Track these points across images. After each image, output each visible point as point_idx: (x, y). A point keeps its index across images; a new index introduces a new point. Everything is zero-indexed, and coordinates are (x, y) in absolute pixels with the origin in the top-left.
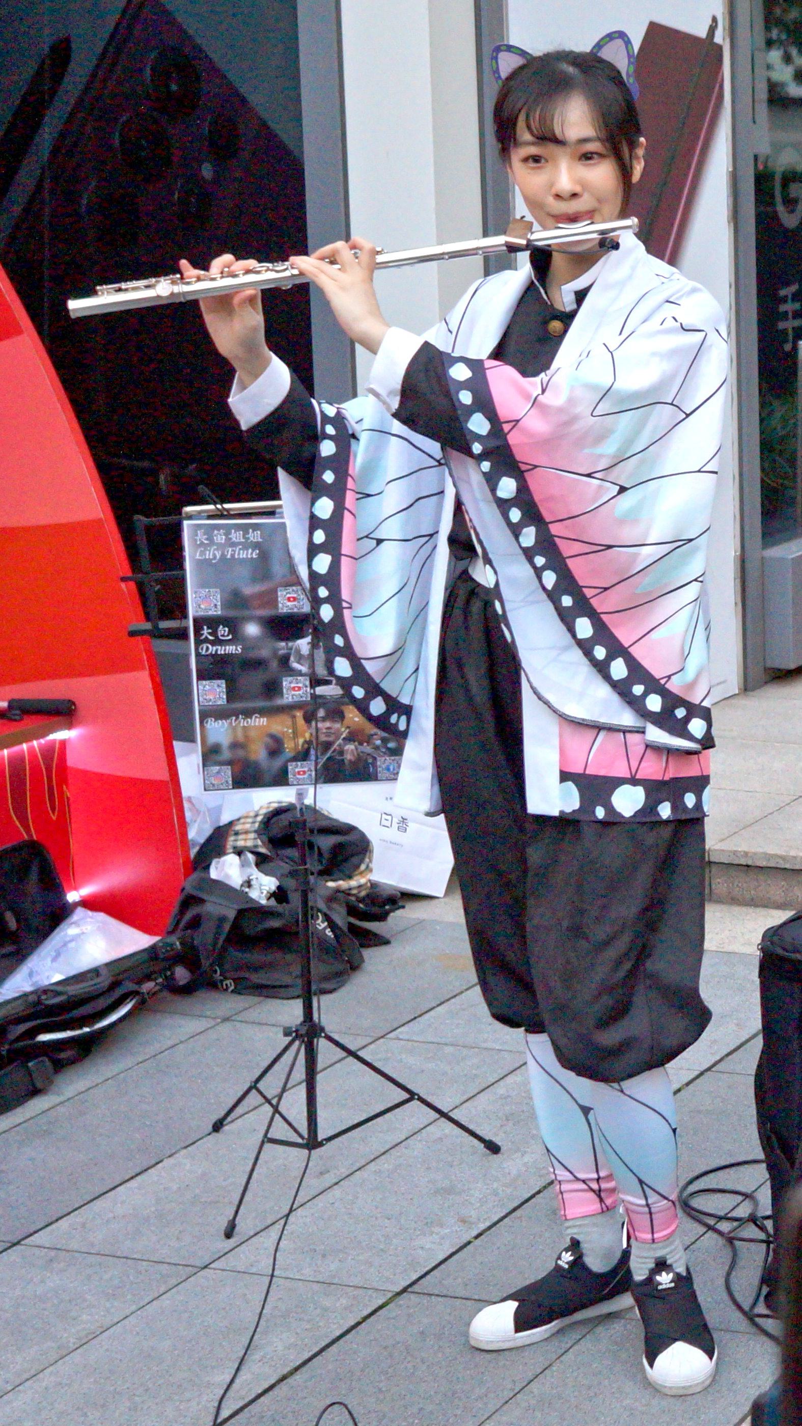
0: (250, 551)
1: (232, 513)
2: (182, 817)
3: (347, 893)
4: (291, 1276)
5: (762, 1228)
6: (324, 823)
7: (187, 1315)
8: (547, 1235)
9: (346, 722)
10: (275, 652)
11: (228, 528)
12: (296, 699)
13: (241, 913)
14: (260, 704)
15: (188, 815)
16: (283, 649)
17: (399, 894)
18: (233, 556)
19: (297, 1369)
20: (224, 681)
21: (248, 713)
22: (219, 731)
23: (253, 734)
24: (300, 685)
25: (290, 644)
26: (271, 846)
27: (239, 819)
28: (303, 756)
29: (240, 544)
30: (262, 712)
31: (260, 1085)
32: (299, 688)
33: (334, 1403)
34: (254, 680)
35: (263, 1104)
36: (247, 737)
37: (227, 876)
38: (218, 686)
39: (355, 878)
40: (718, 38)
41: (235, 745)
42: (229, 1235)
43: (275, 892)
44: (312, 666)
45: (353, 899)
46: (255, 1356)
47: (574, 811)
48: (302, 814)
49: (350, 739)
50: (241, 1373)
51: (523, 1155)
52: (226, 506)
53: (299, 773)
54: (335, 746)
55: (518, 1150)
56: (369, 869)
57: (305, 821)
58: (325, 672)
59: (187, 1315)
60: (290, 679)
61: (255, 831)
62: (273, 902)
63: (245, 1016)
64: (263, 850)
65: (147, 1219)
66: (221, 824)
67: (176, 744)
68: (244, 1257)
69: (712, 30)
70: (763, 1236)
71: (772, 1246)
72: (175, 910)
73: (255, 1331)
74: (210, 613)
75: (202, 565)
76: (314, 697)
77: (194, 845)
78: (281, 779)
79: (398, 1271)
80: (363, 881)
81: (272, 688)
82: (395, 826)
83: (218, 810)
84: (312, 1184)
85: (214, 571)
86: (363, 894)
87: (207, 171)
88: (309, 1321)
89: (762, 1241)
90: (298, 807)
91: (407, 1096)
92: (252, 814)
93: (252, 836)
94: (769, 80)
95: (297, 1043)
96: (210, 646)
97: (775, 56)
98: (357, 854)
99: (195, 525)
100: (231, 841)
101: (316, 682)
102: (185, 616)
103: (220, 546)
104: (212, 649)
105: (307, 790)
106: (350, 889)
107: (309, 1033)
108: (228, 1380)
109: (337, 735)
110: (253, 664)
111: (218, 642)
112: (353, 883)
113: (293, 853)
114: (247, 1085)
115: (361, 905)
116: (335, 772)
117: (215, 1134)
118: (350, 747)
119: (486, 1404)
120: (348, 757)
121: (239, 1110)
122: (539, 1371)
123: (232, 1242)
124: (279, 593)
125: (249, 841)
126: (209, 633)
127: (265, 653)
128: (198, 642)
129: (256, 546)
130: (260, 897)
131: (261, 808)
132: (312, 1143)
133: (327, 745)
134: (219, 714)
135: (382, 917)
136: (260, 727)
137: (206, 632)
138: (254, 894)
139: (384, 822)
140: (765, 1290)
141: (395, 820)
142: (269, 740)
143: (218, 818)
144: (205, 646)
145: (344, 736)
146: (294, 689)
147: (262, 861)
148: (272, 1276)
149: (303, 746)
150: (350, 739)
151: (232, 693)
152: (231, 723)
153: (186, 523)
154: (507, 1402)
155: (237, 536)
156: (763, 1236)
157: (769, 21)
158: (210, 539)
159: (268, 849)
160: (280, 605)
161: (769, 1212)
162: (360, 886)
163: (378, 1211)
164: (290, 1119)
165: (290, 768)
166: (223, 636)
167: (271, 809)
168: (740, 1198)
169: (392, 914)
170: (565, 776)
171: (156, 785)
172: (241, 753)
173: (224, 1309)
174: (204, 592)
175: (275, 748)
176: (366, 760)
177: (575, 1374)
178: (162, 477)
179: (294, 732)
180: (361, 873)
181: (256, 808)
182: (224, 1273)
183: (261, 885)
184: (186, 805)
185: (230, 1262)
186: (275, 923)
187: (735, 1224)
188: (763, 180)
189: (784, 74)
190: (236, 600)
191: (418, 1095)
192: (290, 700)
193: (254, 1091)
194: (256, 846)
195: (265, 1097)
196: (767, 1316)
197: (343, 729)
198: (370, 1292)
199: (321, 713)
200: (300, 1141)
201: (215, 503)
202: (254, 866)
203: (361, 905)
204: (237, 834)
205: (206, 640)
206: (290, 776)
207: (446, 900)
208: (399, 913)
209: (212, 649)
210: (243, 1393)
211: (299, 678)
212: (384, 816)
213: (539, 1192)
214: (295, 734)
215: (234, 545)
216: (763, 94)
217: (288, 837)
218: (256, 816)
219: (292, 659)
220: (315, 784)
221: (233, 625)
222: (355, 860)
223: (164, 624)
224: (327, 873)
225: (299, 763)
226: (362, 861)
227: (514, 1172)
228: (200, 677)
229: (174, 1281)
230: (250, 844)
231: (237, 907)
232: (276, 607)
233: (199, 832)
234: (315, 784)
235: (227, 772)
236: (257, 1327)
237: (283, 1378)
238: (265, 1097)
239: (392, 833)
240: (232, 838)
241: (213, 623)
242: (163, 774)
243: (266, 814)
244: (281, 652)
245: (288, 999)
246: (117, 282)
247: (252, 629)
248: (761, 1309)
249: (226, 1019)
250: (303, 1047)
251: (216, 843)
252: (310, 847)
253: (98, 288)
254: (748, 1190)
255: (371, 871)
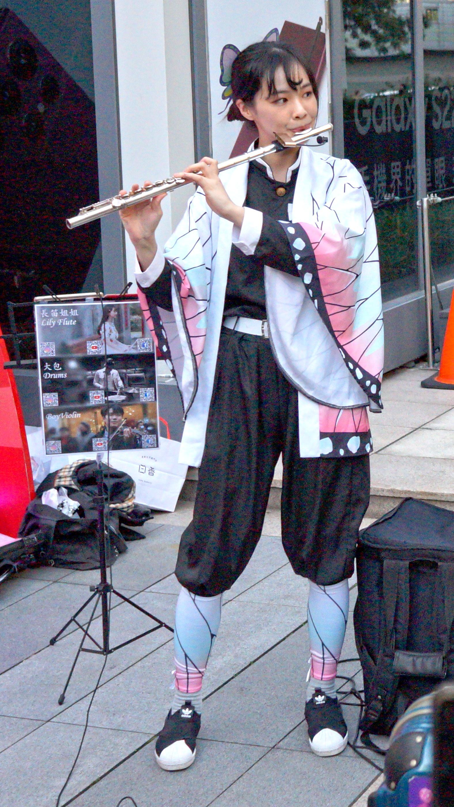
0: (71, 321)
1: (62, 300)
2: (30, 469)
3: (121, 510)
4: (97, 726)
5: (359, 698)
6: (111, 472)
7: (39, 748)
8: (238, 702)
9: (125, 415)
10: (85, 378)
11: (59, 309)
12: (97, 403)
13: (58, 522)
14: (79, 406)
15: (32, 466)
16: (90, 375)
17: (150, 511)
18: (62, 323)
19: (101, 778)
20: (57, 393)
21: (70, 411)
22: (55, 421)
23: (73, 423)
24: (99, 395)
25: (94, 372)
26: (79, 485)
27: (61, 470)
28: (100, 435)
29: (65, 317)
30: (79, 410)
31: (76, 619)
32: (99, 397)
33: (127, 797)
34: (73, 393)
35: (77, 629)
36: (70, 425)
37: (51, 501)
38: (54, 396)
39: (126, 502)
40: (323, 29)
41: (63, 429)
42: (61, 703)
43: (77, 510)
44: (106, 384)
45: (125, 513)
46: (77, 771)
47: (330, 453)
48: (100, 467)
49: (127, 425)
50: (70, 781)
51: (223, 658)
52: (59, 296)
53: (98, 444)
54: (118, 429)
55: (220, 654)
56: (133, 497)
57: (102, 471)
58: (113, 388)
59: (39, 748)
60: (93, 392)
61: (71, 476)
62: (77, 516)
63: (66, 579)
64: (74, 487)
65: (15, 694)
66: (51, 472)
67: (27, 428)
68: (69, 715)
69: (320, 24)
70: (359, 702)
71: (364, 708)
72: (23, 521)
73: (77, 757)
74: (49, 355)
75: (44, 328)
76: (107, 402)
77: (37, 483)
78: (89, 448)
79: (155, 723)
80: (130, 504)
81: (84, 397)
82: (147, 472)
83: (49, 463)
84: (108, 674)
85: (51, 332)
86: (130, 511)
87: (41, 108)
88: (106, 751)
89: (358, 705)
90: (98, 463)
91: (158, 624)
92: (69, 467)
93: (69, 479)
94: (346, 48)
95: (97, 595)
96: (49, 374)
97: (348, 34)
98: (126, 488)
99: (42, 307)
100: (57, 483)
101: (108, 393)
102: (35, 357)
103: (54, 318)
104: (51, 376)
105: (103, 454)
106: (123, 508)
107: (104, 589)
108: (63, 785)
109: (120, 422)
110: (73, 383)
111: (53, 371)
112: (125, 505)
113: (94, 489)
114: (69, 619)
115: (129, 517)
116: (119, 443)
117: (51, 646)
118: (127, 430)
119: (207, 797)
120: (126, 435)
121: (65, 633)
122: (236, 779)
123: (63, 707)
124: (88, 344)
125: (67, 481)
126: (49, 367)
127: (79, 378)
128: (43, 372)
129: (75, 318)
130: (69, 513)
131: (73, 463)
132: (106, 651)
133: (114, 429)
134: (54, 411)
135: (141, 524)
136: (77, 418)
137: (47, 366)
138: (65, 511)
139: (141, 470)
140: (361, 733)
141: (147, 469)
142: (81, 426)
143: (49, 469)
144: (46, 374)
145: (123, 423)
146: (95, 397)
147: (71, 492)
148: (87, 726)
149: (100, 429)
150: (127, 425)
151: (61, 401)
152: (61, 416)
153: (36, 306)
154: (218, 797)
155: (64, 313)
156: (359, 702)
157: (346, 14)
158: (50, 314)
159: (77, 486)
160: (88, 351)
161: (362, 688)
162: (128, 507)
163: (144, 688)
164: (93, 637)
165: (93, 441)
166: (56, 368)
167: (79, 464)
168: (345, 681)
169: (146, 522)
170: (323, 435)
171: (19, 450)
172: (66, 433)
173: (60, 744)
174: (46, 344)
175: (85, 432)
176: (136, 437)
177: (256, 780)
178: (16, 278)
179: (96, 421)
180: (129, 499)
181: (71, 463)
182: (59, 724)
183: (69, 506)
184: (32, 461)
185: (62, 718)
186: (77, 528)
187: (344, 695)
188: (348, 106)
189: (353, 43)
190: (64, 348)
191: (164, 623)
192: (94, 403)
193: (73, 622)
194: (71, 485)
195: (78, 624)
196: (364, 748)
197: (123, 420)
198: (141, 734)
199: (111, 411)
200: (98, 649)
201: (52, 295)
202: (67, 496)
203: (129, 517)
204: (60, 478)
205: (47, 371)
206: (94, 446)
207: (176, 513)
208: (150, 521)
209: (51, 376)
210: (72, 791)
211: (99, 391)
212: (141, 467)
213: (233, 678)
214: (97, 424)
215: (63, 318)
216: (343, 56)
217: (94, 482)
218: (71, 468)
219: (95, 380)
220: (108, 450)
221: (61, 361)
222: (125, 492)
223: (23, 362)
224: (112, 500)
225: (99, 439)
226: (130, 492)
227: (218, 667)
228: (44, 391)
229: (31, 729)
230: (67, 483)
231: (56, 520)
232: (86, 352)
233: (38, 476)
234: (108, 450)
235: (59, 444)
236: (78, 754)
237: (94, 783)
238: (78, 624)
239: (146, 476)
240: (57, 480)
241: (52, 361)
242: (20, 445)
243: (76, 466)
244: (89, 377)
245: (91, 569)
246: (88, 205)
247: (73, 365)
248: (359, 743)
249: (55, 582)
250: (101, 598)
251: (49, 482)
252: (101, 485)
253: (81, 209)
254: (349, 676)
255: (134, 498)
